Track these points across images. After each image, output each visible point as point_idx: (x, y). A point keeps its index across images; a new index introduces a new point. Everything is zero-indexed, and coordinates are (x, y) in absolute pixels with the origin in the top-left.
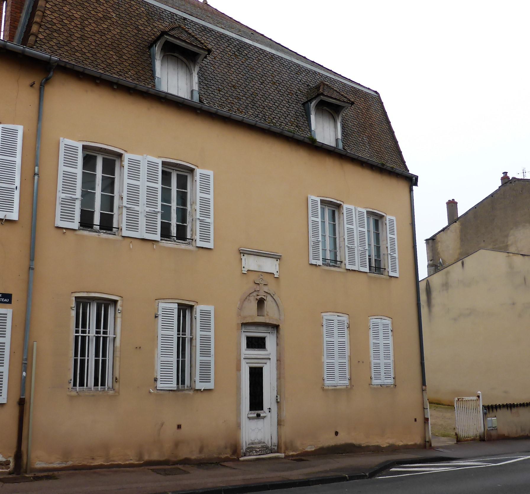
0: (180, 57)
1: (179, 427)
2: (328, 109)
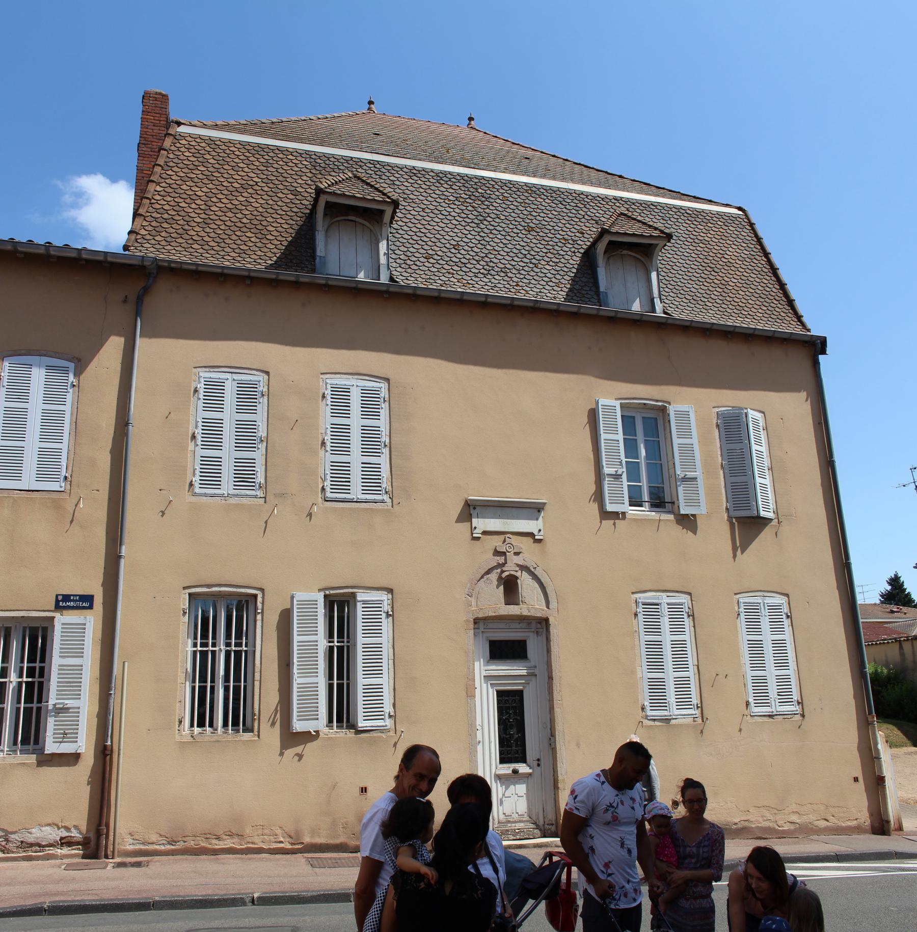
0: (358, 220)
1: (364, 790)
2: (630, 253)
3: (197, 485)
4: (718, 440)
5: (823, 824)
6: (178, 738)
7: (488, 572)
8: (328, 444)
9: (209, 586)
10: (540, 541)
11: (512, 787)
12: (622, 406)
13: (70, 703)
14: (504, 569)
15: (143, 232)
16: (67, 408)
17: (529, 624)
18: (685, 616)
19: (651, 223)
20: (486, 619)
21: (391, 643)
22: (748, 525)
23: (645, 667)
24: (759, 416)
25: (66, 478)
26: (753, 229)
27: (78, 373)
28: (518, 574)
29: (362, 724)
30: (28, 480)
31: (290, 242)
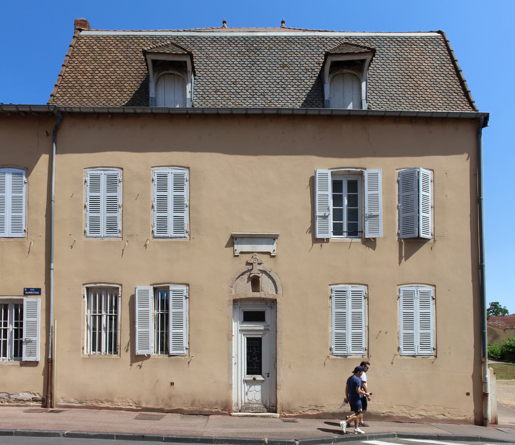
0: (175, 72)
1: (172, 384)
2: (349, 71)
3: (88, 232)
4: (397, 191)
5: (441, 417)
6: (82, 356)
7: (243, 274)
8: (156, 207)
9: (95, 283)
10: (274, 256)
11: (253, 387)
12: (333, 174)
13: (33, 339)
14: (251, 272)
15: (58, 95)
16: (24, 195)
17: (267, 303)
18: (363, 298)
19: (363, 44)
20: (241, 300)
21: (188, 312)
22: (411, 242)
23: (334, 327)
24: (429, 173)
25: (25, 230)
26: (447, 45)
27: (27, 176)
28: (260, 275)
29: (171, 352)
30: (8, 232)
31: (136, 92)
